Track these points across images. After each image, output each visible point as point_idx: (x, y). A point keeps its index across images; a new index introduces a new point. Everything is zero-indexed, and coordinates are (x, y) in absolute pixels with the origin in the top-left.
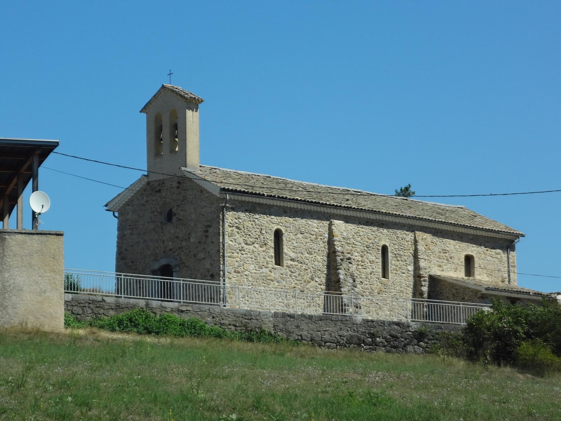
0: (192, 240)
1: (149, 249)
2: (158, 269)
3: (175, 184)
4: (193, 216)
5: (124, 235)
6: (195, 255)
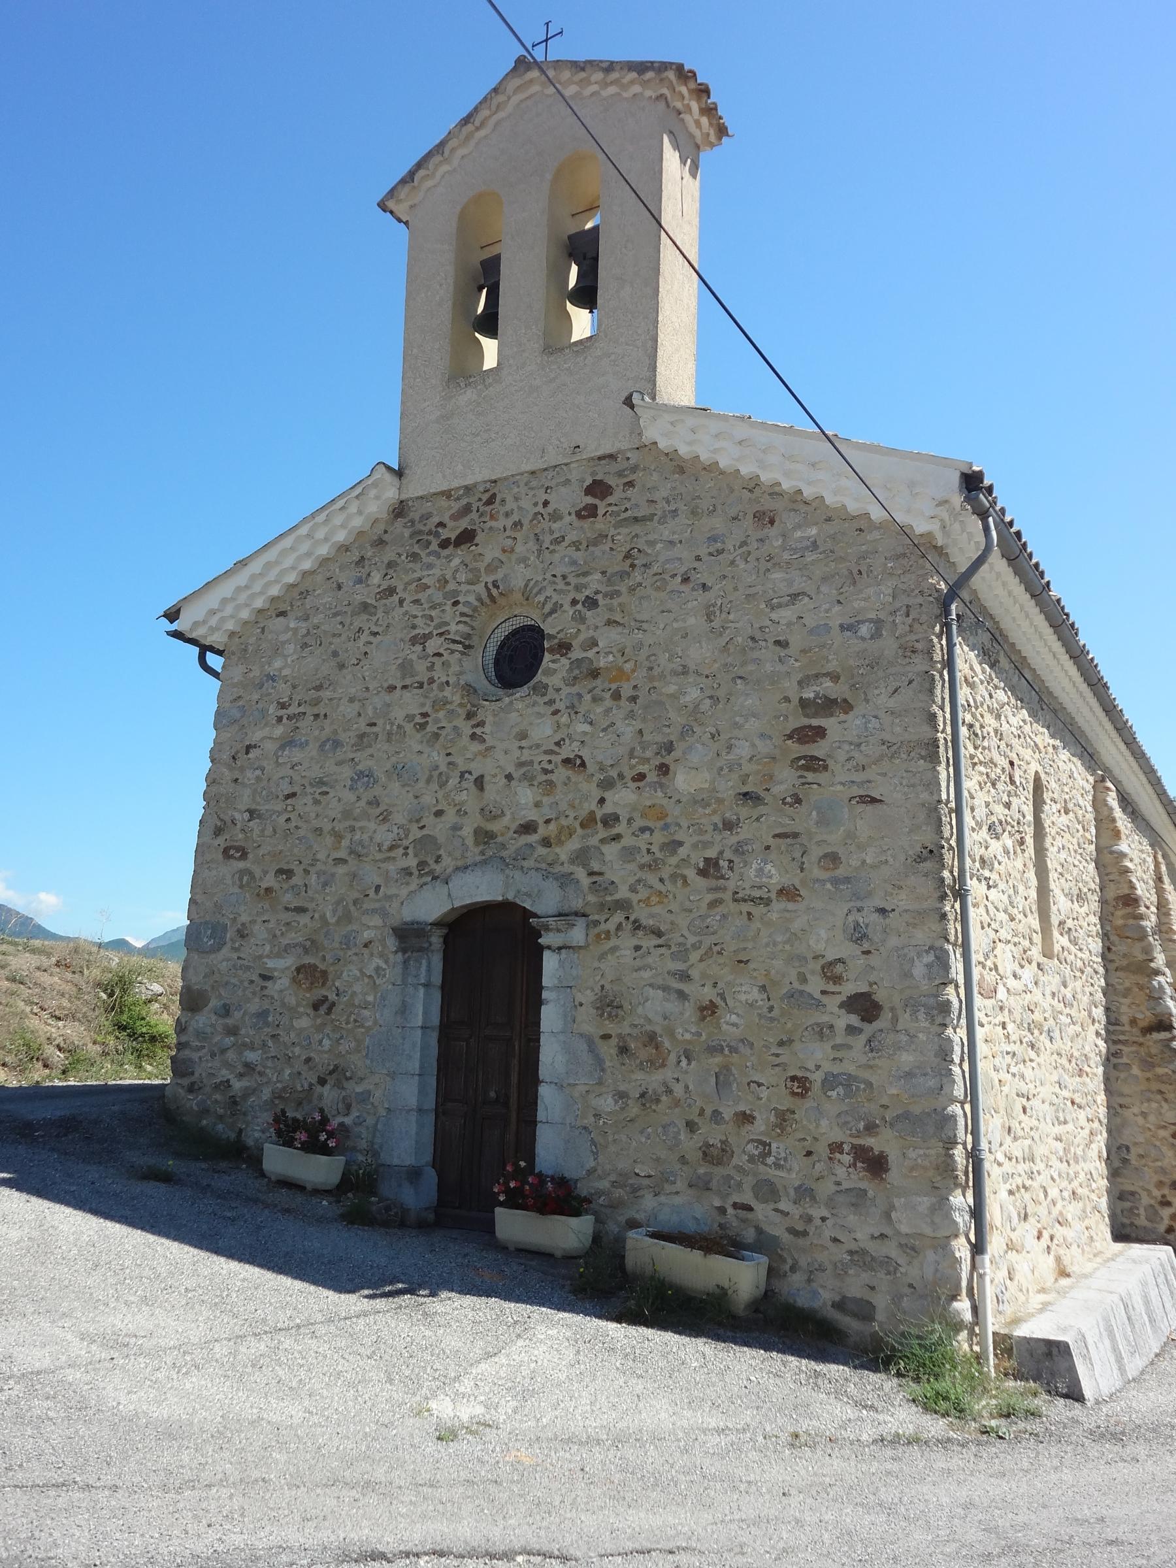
0: (684, 781)
1: (385, 818)
2: (437, 924)
3: (569, 498)
4: (700, 653)
5: (248, 748)
6: (710, 868)
